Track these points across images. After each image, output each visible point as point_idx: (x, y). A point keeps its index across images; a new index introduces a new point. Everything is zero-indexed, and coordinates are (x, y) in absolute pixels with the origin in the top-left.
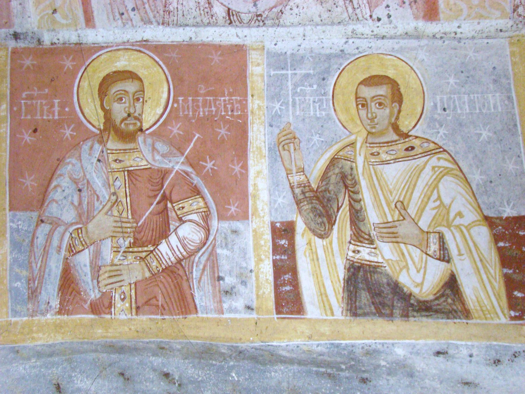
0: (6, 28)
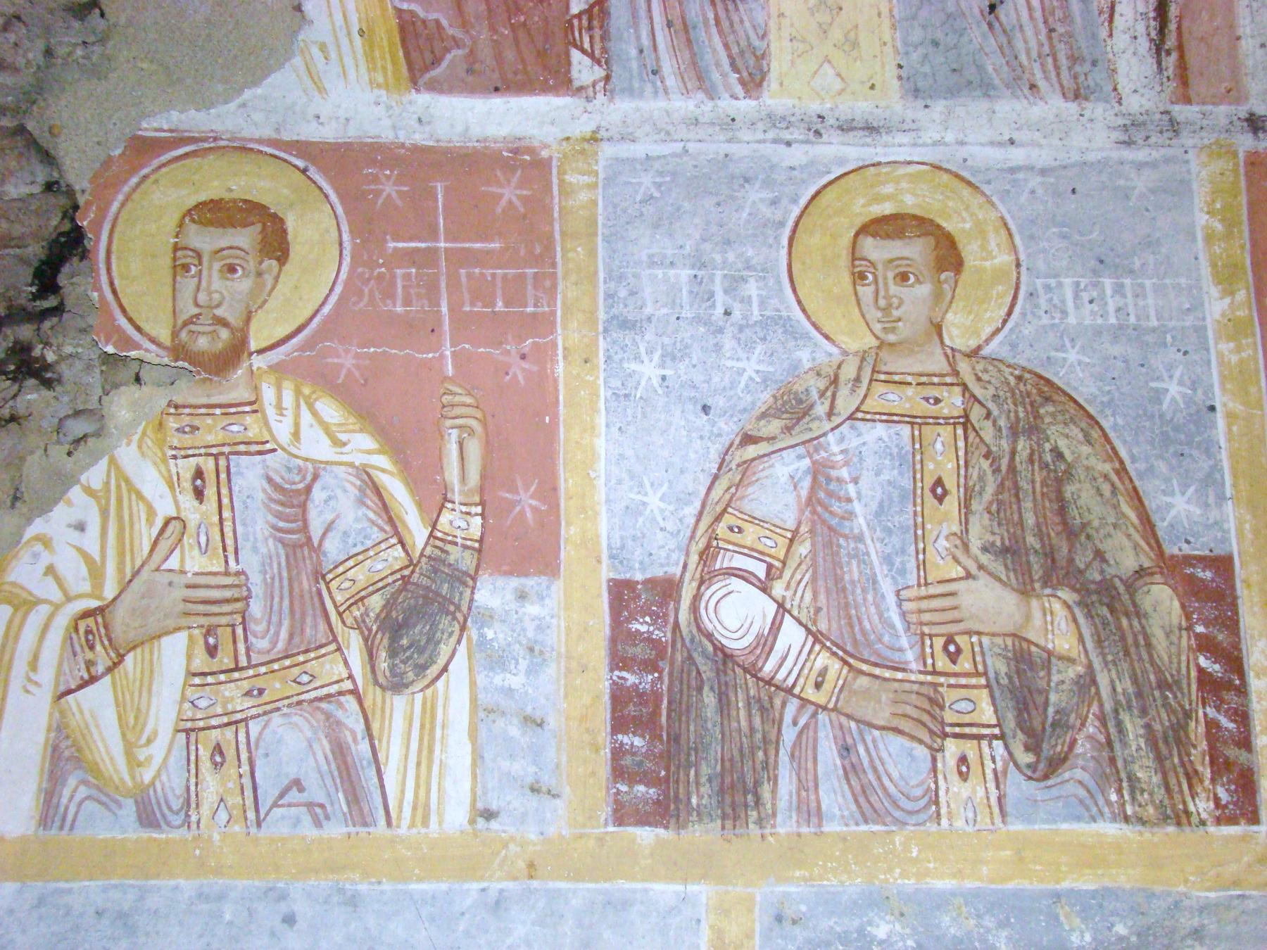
0: (1230, 104)
